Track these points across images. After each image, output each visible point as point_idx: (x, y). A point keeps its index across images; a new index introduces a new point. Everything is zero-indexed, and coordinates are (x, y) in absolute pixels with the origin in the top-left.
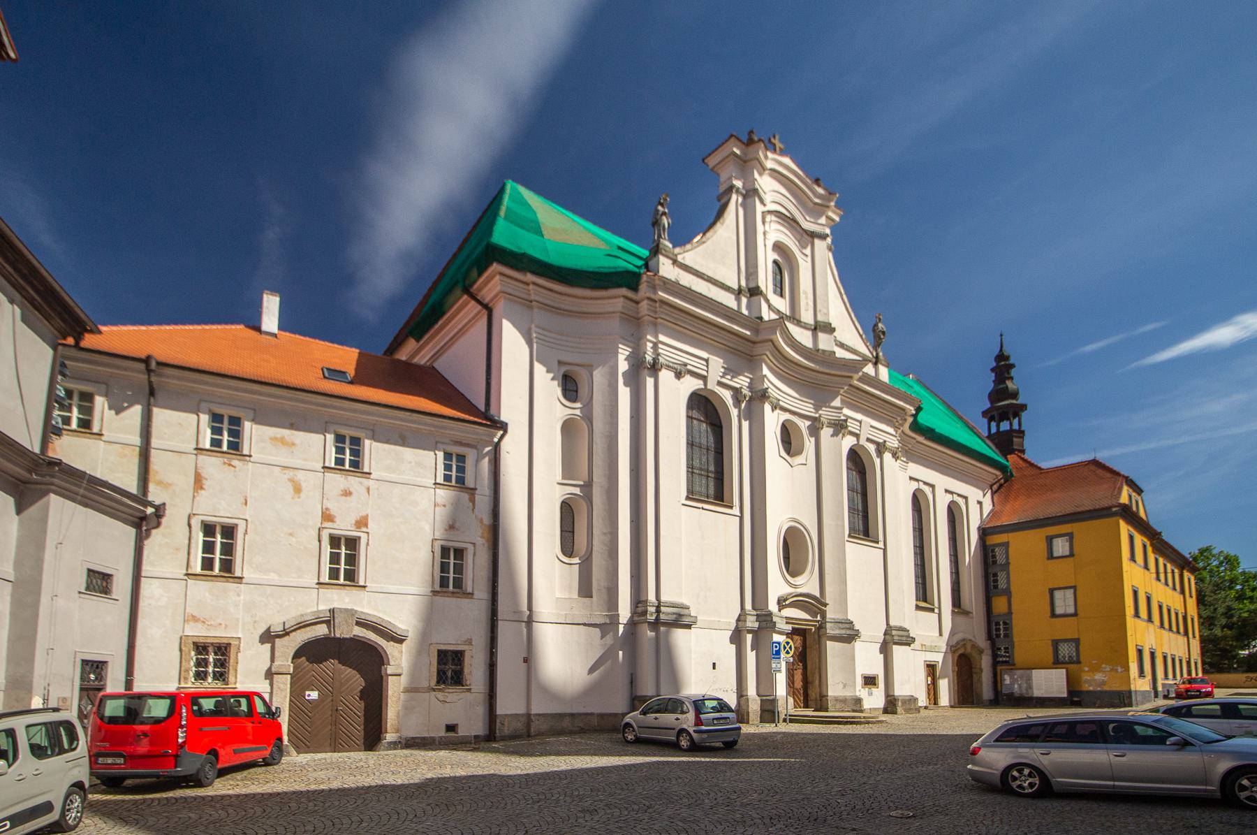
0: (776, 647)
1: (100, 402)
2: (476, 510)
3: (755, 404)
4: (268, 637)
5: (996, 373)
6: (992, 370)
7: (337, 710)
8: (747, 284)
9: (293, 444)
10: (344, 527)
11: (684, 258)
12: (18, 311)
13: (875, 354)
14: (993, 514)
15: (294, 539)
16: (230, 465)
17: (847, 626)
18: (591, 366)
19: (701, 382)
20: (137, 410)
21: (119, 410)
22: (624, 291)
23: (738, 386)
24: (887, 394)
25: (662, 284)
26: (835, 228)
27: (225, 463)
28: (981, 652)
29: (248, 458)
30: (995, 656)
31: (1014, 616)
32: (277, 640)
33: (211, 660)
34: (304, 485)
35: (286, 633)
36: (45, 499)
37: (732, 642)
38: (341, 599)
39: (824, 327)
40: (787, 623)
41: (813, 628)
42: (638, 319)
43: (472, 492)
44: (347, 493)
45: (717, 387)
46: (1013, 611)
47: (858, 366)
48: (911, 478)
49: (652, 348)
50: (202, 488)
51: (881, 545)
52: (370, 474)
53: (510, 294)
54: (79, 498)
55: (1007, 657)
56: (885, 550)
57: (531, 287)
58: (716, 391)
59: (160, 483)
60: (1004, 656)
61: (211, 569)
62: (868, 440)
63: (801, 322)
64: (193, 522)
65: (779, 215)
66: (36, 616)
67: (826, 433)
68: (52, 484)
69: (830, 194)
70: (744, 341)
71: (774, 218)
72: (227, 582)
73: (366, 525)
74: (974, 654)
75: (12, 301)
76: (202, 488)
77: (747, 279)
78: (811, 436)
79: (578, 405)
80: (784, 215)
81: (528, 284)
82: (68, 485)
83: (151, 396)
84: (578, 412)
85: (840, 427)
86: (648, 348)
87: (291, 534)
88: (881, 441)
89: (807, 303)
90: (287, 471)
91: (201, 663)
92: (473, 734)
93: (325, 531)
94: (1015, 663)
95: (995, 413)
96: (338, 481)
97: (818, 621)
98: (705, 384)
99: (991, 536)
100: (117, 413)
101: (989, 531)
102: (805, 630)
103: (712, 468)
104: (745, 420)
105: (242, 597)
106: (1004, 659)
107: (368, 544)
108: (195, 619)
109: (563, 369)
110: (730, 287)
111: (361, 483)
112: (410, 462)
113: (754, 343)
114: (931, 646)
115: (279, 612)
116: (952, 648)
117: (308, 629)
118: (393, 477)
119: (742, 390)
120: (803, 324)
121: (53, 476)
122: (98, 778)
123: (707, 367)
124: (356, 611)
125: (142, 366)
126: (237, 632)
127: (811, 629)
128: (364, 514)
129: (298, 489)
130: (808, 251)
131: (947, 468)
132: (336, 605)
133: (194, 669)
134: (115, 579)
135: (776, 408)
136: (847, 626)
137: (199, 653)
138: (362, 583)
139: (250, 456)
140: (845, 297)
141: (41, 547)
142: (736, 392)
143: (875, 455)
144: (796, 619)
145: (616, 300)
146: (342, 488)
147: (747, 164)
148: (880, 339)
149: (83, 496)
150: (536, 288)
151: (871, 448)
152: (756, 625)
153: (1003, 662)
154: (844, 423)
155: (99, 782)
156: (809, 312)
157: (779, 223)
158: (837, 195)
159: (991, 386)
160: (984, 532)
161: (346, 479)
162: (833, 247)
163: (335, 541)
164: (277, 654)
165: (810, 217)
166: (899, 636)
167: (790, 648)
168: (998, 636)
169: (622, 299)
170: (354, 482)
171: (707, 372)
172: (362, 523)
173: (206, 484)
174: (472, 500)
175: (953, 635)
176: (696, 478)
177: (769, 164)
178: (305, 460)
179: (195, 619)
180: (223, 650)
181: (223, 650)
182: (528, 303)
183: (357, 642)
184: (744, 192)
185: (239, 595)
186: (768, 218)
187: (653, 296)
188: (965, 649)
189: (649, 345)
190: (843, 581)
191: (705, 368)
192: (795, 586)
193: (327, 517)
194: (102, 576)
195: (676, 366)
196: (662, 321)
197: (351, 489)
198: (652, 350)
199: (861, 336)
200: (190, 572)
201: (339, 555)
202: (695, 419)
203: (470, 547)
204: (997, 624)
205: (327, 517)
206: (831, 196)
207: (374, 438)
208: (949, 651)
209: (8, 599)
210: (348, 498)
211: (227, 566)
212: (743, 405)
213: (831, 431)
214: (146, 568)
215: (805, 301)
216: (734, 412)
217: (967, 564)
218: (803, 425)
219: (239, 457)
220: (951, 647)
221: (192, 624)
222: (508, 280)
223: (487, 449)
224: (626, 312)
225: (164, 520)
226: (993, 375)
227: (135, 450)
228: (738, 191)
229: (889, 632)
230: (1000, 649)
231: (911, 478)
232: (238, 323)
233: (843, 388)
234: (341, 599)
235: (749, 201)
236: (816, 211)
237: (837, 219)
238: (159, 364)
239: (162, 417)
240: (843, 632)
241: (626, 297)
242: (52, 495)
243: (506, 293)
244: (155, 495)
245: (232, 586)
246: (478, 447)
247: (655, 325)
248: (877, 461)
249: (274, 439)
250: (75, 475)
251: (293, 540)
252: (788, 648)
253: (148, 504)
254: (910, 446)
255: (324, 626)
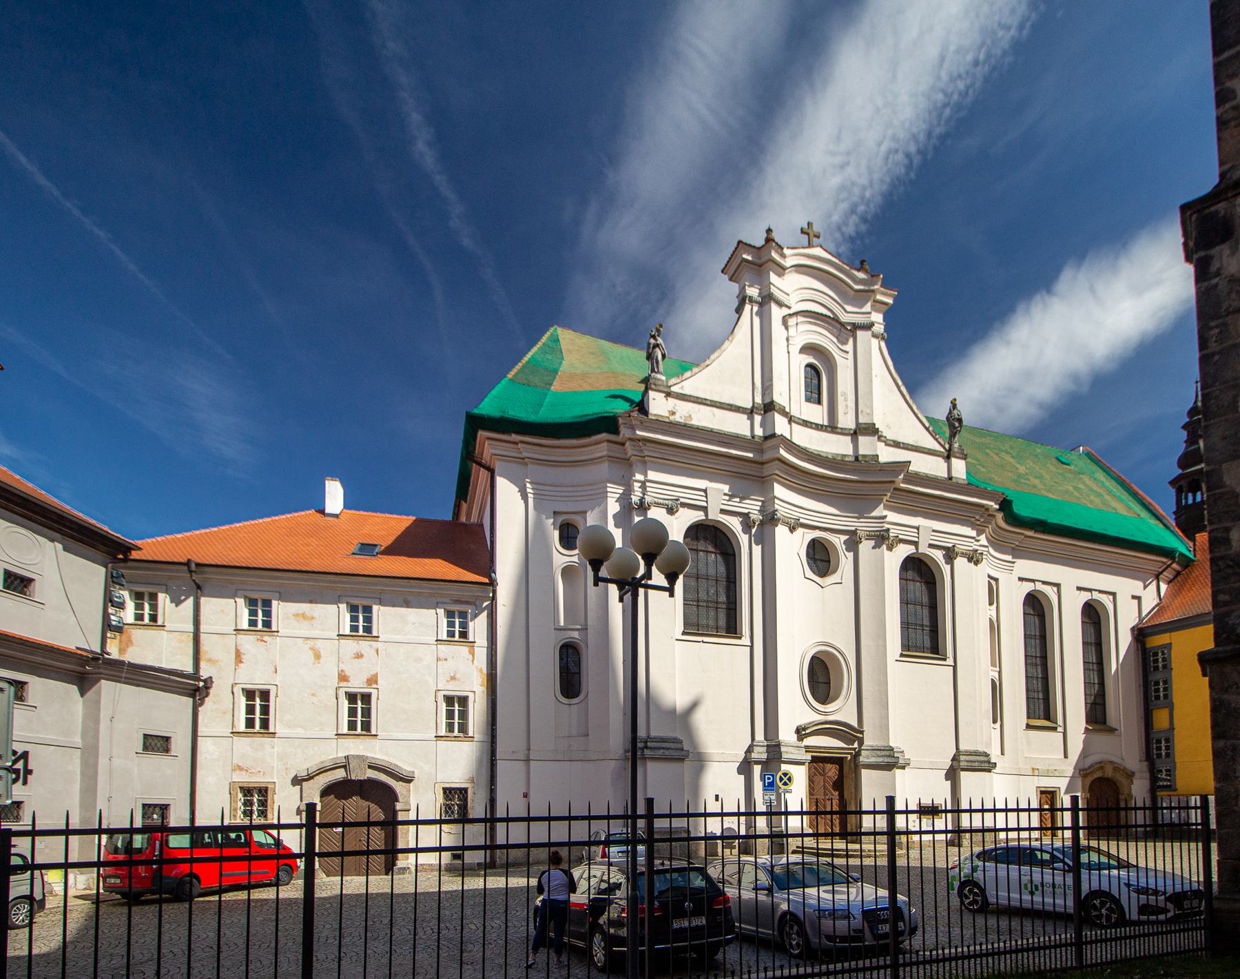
0: (769, 779)
1: (162, 597)
2: (475, 661)
3: (767, 528)
4: (297, 781)
5: (1188, 432)
6: (1184, 427)
7: (360, 840)
8: (763, 400)
9: (313, 618)
10: (358, 685)
11: (682, 388)
12: (59, 546)
13: (947, 446)
14: (1161, 608)
15: (315, 698)
16: (262, 641)
17: (887, 753)
18: (585, 512)
19: (913, 547)
20: (189, 603)
21: (177, 602)
22: (604, 436)
23: (746, 511)
24: (953, 493)
25: (639, 423)
26: (890, 315)
27: (258, 640)
28: (1130, 775)
29: (276, 634)
30: (1154, 779)
31: (1176, 731)
32: (304, 783)
33: (255, 800)
34: (322, 652)
35: (310, 778)
36: (98, 685)
37: (740, 772)
38: (357, 747)
39: (865, 429)
40: (806, 751)
41: (849, 757)
42: (628, 460)
43: (472, 644)
44: (359, 656)
45: (721, 515)
46: (1175, 726)
47: (897, 469)
48: (1021, 579)
49: (640, 487)
50: (241, 662)
51: (950, 661)
52: (378, 637)
53: (502, 456)
54: (123, 680)
55: (1169, 780)
56: (955, 667)
57: (520, 446)
58: (927, 553)
59: (209, 660)
60: (1166, 780)
61: (253, 727)
62: (931, 546)
63: (837, 428)
64: (235, 690)
65: (806, 314)
66: (96, 772)
67: (865, 547)
68: (100, 673)
69: (872, 276)
70: (750, 464)
71: (801, 319)
72: (264, 737)
73: (376, 682)
74: (1120, 778)
75: (52, 540)
76: (241, 662)
77: (763, 395)
78: (848, 550)
79: (576, 552)
80: (822, 314)
81: (516, 443)
82: (116, 673)
83: (198, 590)
84: (575, 559)
85: (882, 538)
86: (636, 489)
87: (313, 695)
88: (950, 545)
89: (847, 406)
90: (308, 642)
91: (248, 803)
92: (476, 862)
93: (341, 689)
94: (1177, 787)
95: (1182, 483)
96: (351, 646)
97: (855, 749)
98: (917, 549)
99: (1156, 637)
100: (177, 606)
101: (1149, 631)
102: (842, 758)
103: (723, 598)
104: (757, 545)
105: (276, 749)
106: (1165, 783)
107: (378, 699)
108: (240, 768)
109: (561, 519)
110: (740, 407)
111: (371, 646)
112: (414, 624)
113: (763, 463)
114: (1048, 770)
115: (305, 760)
116: (1082, 771)
117: (329, 773)
118: (399, 638)
119: (751, 515)
120: (839, 431)
121: (99, 668)
122: (117, 893)
123: (706, 497)
124: (367, 757)
125: (185, 568)
126: (273, 778)
127: (847, 757)
128: (374, 673)
129: (318, 656)
130: (849, 347)
131: (1080, 561)
132: (352, 753)
133: (242, 808)
134: (173, 740)
135: (794, 528)
136: (887, 753)
137: (245, 795)
138: (373, 733)
139: (278, 632)
140: (903, 389)
141: (97, 721)
142: (746, 519)
143: (943, 561)
144: (825, 748)
145: (600, 445)
146: (354, 652)
147: (763, 267)
148: (955, 428)
149: (125, 678)
150: (524, 446)
151: (938, 555)
152: (764, 756)
153: (1163, 787)
154: (885, 534)
155: (119, 896)
156: (849, 415)
157: (810, 323)
158: (881, 276)
159: (1181, 448)
160: (1141, 634)
161: (358, 643)
162: (885, 334)
163: (352, 698)
164: (304, 795)
165: (853, 305)
166: (968, 761)
167: (781, 779)
168: (1159, 756)
169: (605, 444)
170: (365, 646)
171: (707, 502)
172: (373, 680)
173: (244, 658)
174: (472, 653)
175: (1084, 758)
176: (703, 611)
177: (788, 262)
178: (323, 630)
179: (240, 768)
180: (263, 791)
181: (263, 791)
182: (522, 461)
183: (371, 782)
184: (760, 299)
185: (273, 747)
186: (792, 322)
187: (633, 437)
188: (1104, 772)
189: (637, 485)
190: (885, 705)
191: (704, 499)
192: (826, 714)
193: (343, 678)
194: (1044, 655)
195: (667, 502)
196: (649, 458)
197: (363, 652)
198: (640, 490)
199: (927, 429)
200: (234, 731)
201: (254, 706)
202: (701, 551)
203: (471, 696)
204: (1159, 741)
205: (343, 678)
206: (875, 278)
207: (381, 603)
208: (1077, 775)
209: (78, 761)
210: (360, 660)
211: (265, 724)
212: (754, 531)
213: (872, 543)
214: (202, 730)
215: (845, 403)
216: (744, 539)
217: (1113, 672)
218: (838, 541)
219: (268, 633)
220: (1080, 770)
221: (237, 772)
222: (496, 443)
223: (485, 604)
224: (612, 454)
225: (212, 691)
226: (1185, 433)
227: (189, 636)
228: (751, 300)
229: (957, 757)
230: (1161, 771)
231: (1021, 579)
232: (308, 509)
233: (886, 495)
234: (357, 747)
235: (766, 308)
236: (860, 298)
237: (890, 301)
238: (198, 565)
239: (208, 604)
240: (881, 759)
241: (609, 441)
242: (103, 681)
243: (496, 455)
244: (204, 674)
245: (267, 740)
246: (477, 603)
247: (645, 463)
248: (946, 569)
249: (297, 615)
250: (118, 664)
251: (315, 699)
252: (785, 779)
253: (199, 679)
254: (1017, 543)
255: (343, 770)
